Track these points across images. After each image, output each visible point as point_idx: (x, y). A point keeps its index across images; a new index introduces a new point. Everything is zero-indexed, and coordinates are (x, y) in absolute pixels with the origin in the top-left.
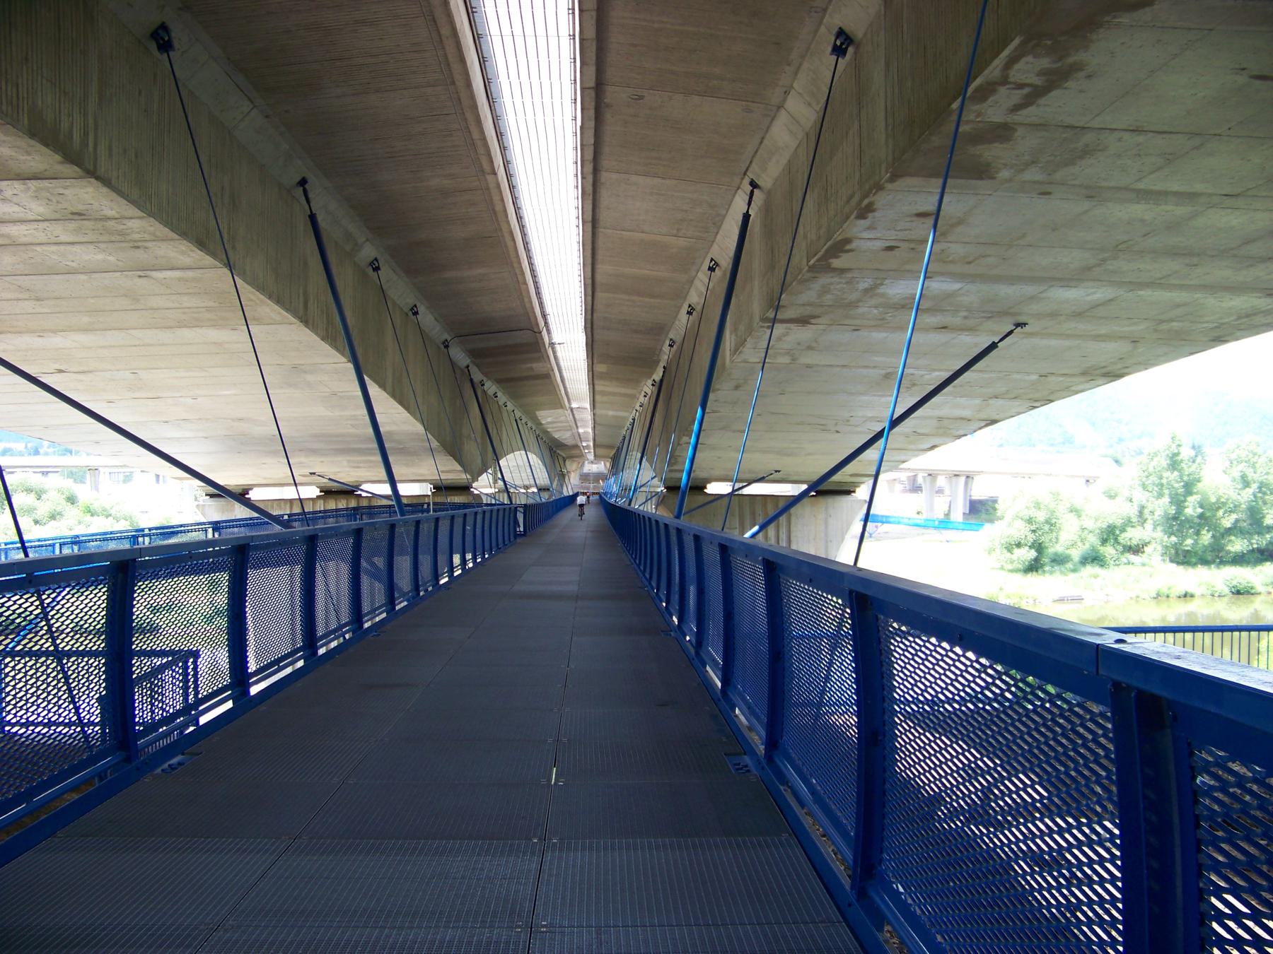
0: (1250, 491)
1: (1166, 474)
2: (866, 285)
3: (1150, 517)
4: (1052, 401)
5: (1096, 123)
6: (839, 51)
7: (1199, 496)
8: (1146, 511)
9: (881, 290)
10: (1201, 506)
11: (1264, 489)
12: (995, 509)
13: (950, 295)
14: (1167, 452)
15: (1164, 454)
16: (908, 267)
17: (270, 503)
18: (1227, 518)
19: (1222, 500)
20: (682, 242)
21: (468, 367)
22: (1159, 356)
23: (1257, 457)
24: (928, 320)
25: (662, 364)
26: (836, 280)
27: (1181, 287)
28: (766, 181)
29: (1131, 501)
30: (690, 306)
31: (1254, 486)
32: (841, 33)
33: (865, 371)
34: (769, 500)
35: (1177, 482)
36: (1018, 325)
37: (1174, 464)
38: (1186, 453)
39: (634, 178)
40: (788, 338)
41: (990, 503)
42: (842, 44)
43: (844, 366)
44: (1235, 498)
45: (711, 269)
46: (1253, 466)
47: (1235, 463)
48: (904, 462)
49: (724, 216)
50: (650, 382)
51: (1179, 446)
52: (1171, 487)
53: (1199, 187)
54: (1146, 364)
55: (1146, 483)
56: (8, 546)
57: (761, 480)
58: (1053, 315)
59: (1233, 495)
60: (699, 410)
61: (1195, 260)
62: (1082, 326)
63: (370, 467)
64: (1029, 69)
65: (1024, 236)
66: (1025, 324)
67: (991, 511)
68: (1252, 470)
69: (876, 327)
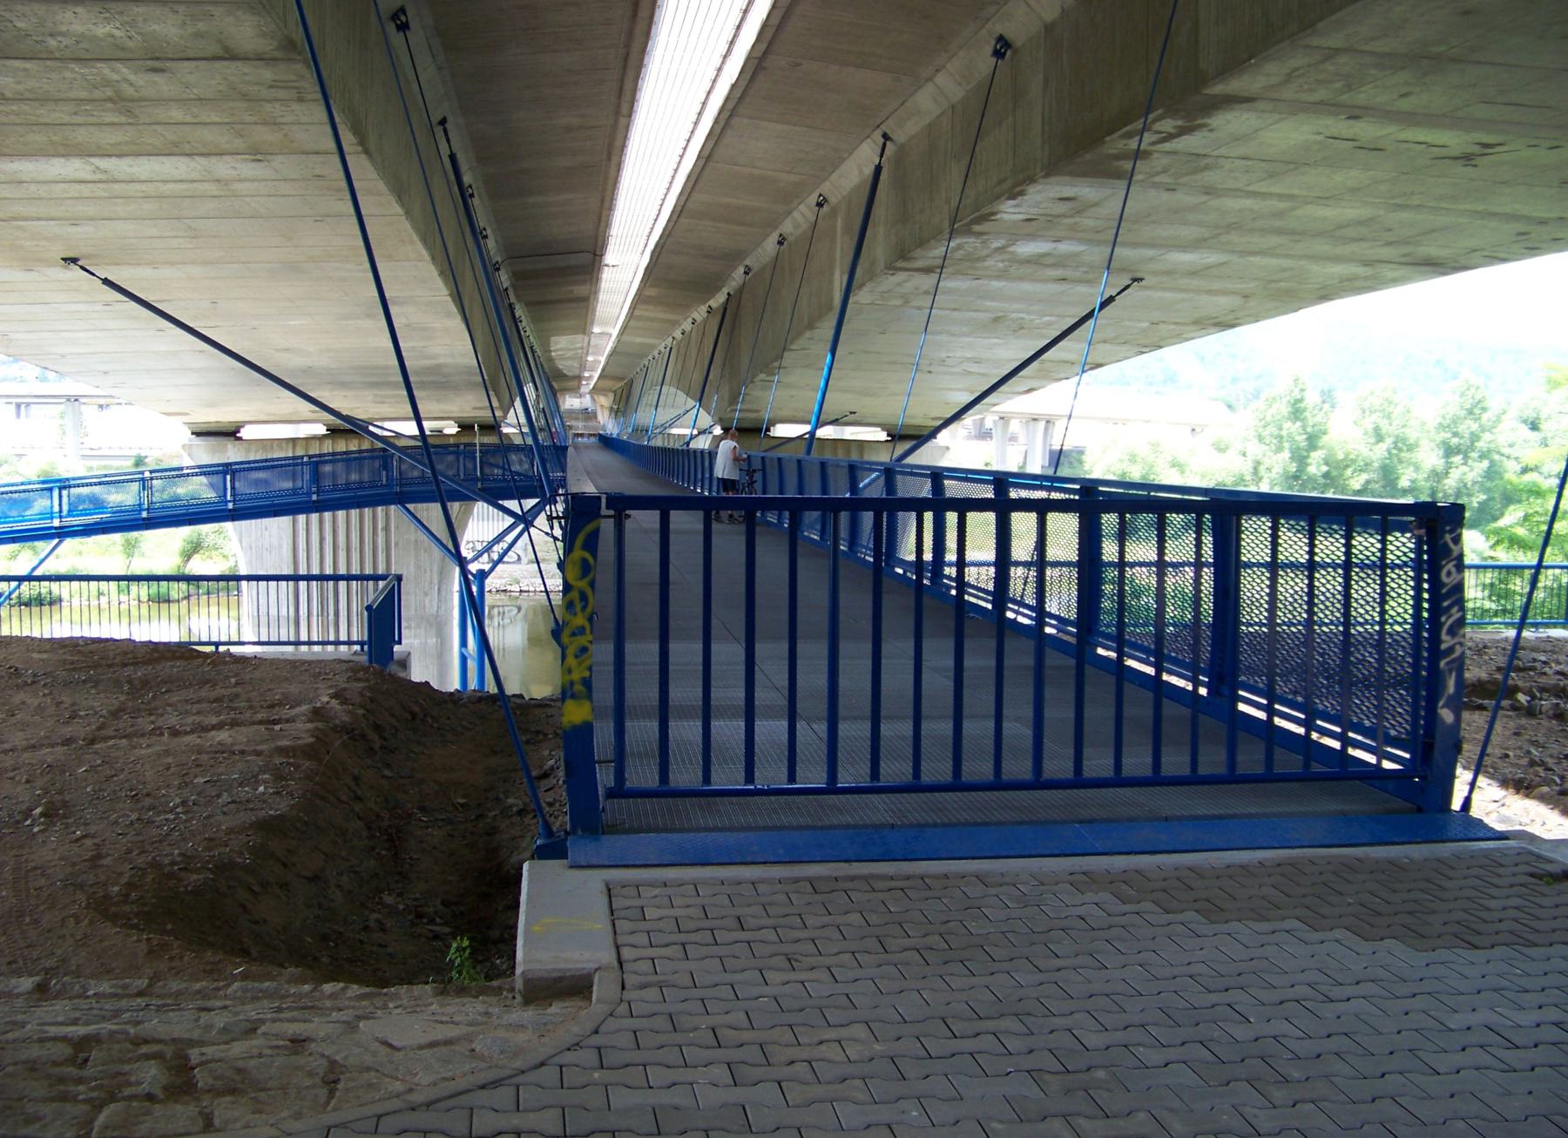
1: (1287, 425)
2: (999, 245)
3: (1266, 476)
4: (1161, 347)
5: (1216, 153)
6: (998, 54)
7: (1324, 451)
8: (1262, 469)
9: (1011, 249)
10: (1327, 464)
11: (1400, 445)
12: (1081, 462)
13: (1077, 255)
14: (1289, 398)
15: (1285, 400)
16: (1040, 233)
17: (269, 443)
18: (1356, 479)
19: (1352, 456)
20: (793, 178)
21: (507, 289)
22: (1269, 310)
23: (1392, 406)
24: (1049, 273)
25: (725, 290)
26: (972, 240)
27: (1287, 256)
28: (900, 136)
29: (1244, 455)
30: (781, 235)
31: (1389, 441)
32: (1001, 39)
33: (974, 315)
34: (839, 444)
35: (1301, 434)
36: (1135, 280)
37: (1297, 413)
38: (1312, 399)
39: (765, 124)
40: (908, 285)
41: (1074, 454)
42: (1001, 47)
43: (955, 309)
44: (1366, 455)
45: (820, 205)
46: (1389, 417)
47: (1367, 412)
48: (995, 405)
49: (845, 160)
50: (703, 309)
51: (1302, 390)
52: (1291, 438)
53: (1296, 192)
54: (1257, 318)
55: (1263, 434)
58: (1169, 273)
59: (1365, 452)
60: (829, 357)
61: (1297, 238)
62: (1195, 283)
63: (398, 403)
64: (1168, 125)
65: (1149, 215)
66: (1142, 279)
67: (1076, 464)
68: (1386, 421)
69: (998, 277)
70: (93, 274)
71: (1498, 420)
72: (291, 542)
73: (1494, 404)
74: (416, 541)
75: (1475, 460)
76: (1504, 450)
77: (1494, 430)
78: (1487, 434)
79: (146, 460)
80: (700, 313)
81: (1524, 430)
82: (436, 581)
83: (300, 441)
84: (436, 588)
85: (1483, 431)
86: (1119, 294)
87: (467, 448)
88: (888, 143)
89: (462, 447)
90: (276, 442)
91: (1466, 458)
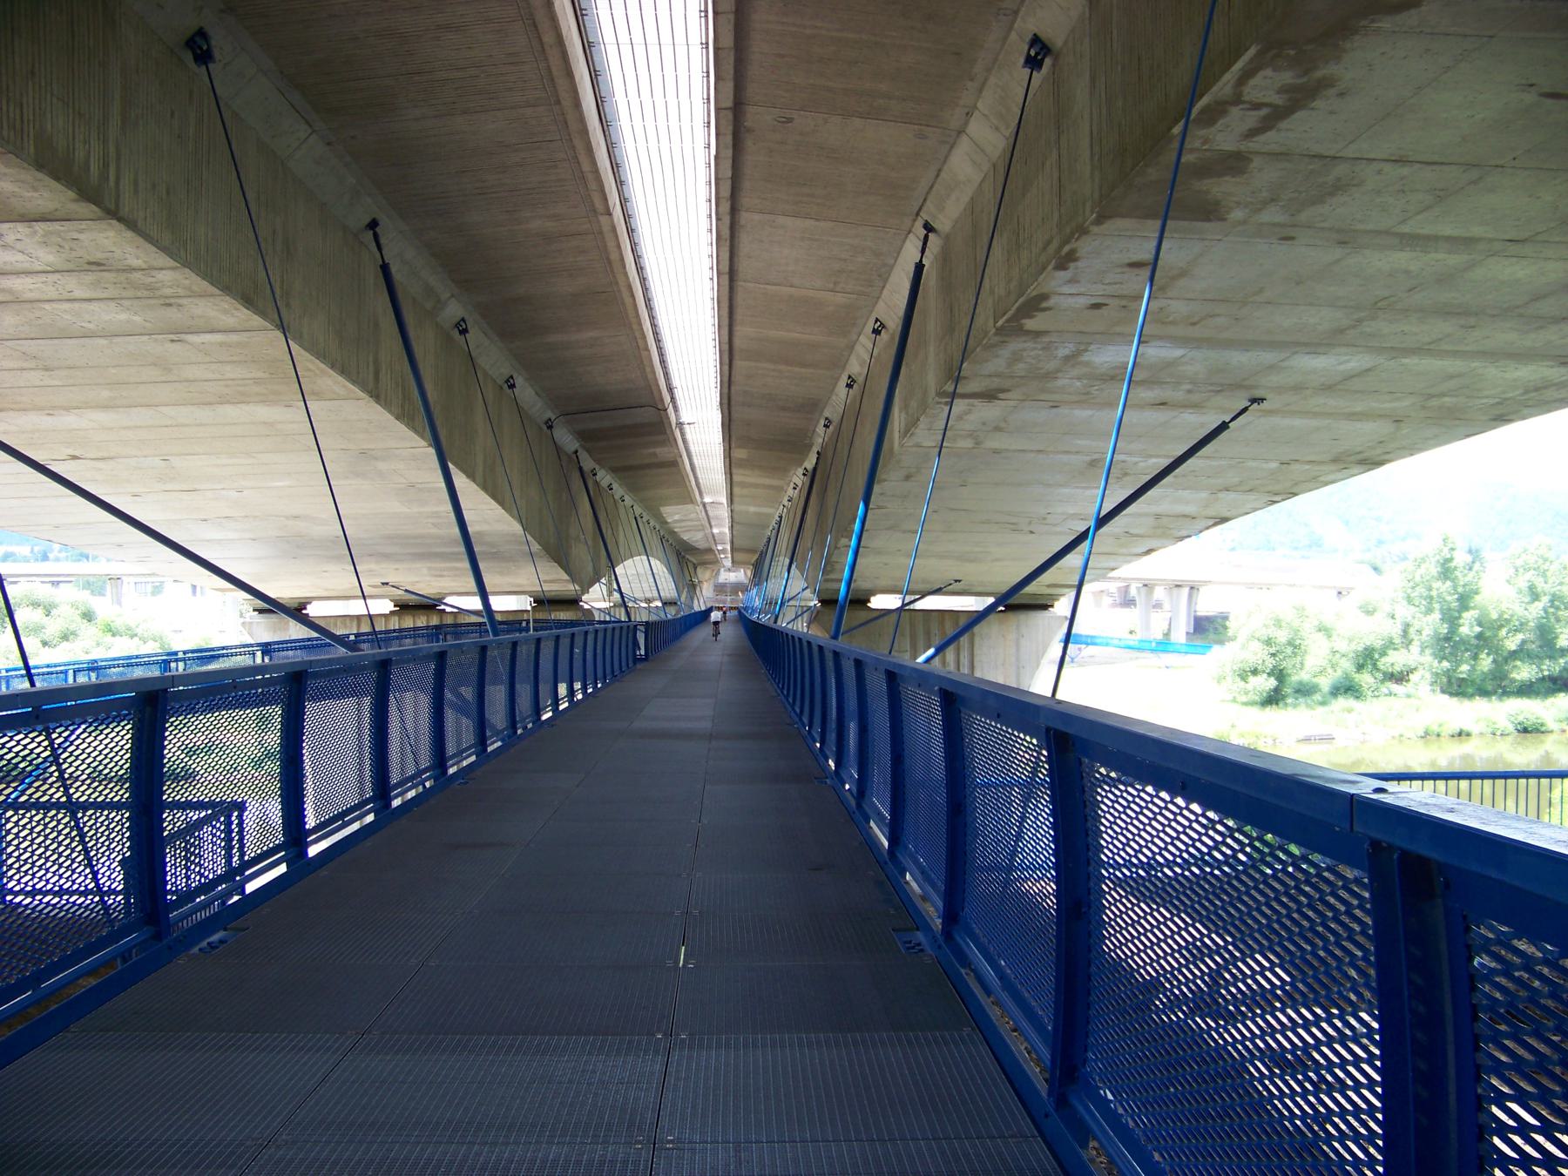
0: (1539, 605)
1: (1436, 584)
2: (1067, 352)
3: (1416, 638)
4: (1295, 494)
6: (1033, 63)
7: (1477, 611)
8: (1412, 630)
9: (1085, 358)
10: (1480, 624)
11: (1556, 603)
12: (1225, 628)
13: (1170, 364)
14: (1438, 557)
15: (1434, 560)
16: (1118, 329)
17: (332, 620)
18: (1511, 639)
19: (1506, 616)
20: (840, 299)
21: (576, 452)
22: (1427, 439)
23: (1548, 563)
24: (1143, 395)
25: (815, 449)
27: (1455, 354)
28: (943, 224)
29: (1393, 617)
30: (850, 377)
31: (1545, 600)
32: (1036, 40)
33: (1065, 458)
34: (947, 616)
35: (1450, 594)
36: (1254, 401)
37: (1446, 572)
38: (1461, 559)
39: (781, 220)
40: (971, 417)
41: (1219, 620)
42: (1037, 54)
43: (1040, 451)
44: (1521, 614)
45: (876, 332)
46: (1544, 574)
47: (1521, 570)
48: (1113, 569)
49: (892, 267)
50: (800, 471)
51: (1453, 549)
52: (1442, 600)
53: (1477, 231)
54: (1412, 449)
55: (1412, 595)
56: (10, 673)
57: (938, 591)
58: (1298, 388)
59: (1519, 610)
60: (861, 506)
61: (1472, 321)
62: (1333, 402)
63: (456, 576)
64: (1267, 85)
65: (1261, 290)
66: (1263, 400)
67: (1221, 629)
69: (1079, 403)
80: (798, 478)
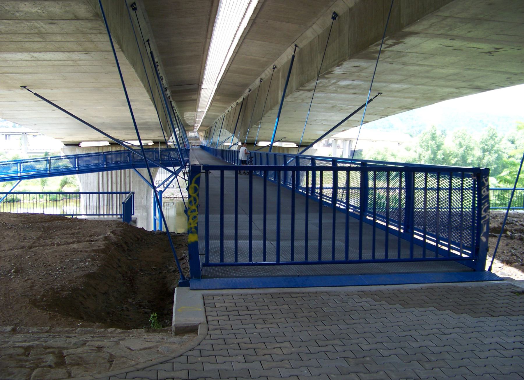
1: (430, 142)
2: (334, 82)
3: (423, 159)
4: (388, 116)
6: (334, 18)
7: (443, 151)
8: (422, 157)
9: (338, 83)
10: (443, 155)
11: (468, 149)
12: (361, 154)
13: (360, 85)
14: (431, 133)
15: (429, 134)
16: (347, 78)
17: (90, 148)
18: (453, 160)
19: (452, 152)
20: (265, 59)
21: (169, 96)
22: (424, 103)
23: (465, 136)
24: (351, 91)
25: (242, 97)
27: (430, 86)
28: (301, 46)
29: (416, 152)
30: (261, 79)
31: (464, 147)
32: (334, 13)
33: (326, 105)
34: (280, 148)
35: (435, 145)
36: (379, 93)
37: (433, 138)
38: (438, 133)
39: (256, 41)
40: (303, 95)
41: (359, 152)
42: (335, 16)
43: (319, 103)
44: (456, 152)
45: (274, 68)
46: (464, 139)
47: (457, 138)
48: (332, 135)
49: (282, 53)
50: (235, 103)
51: (435, 130)
52: (431, 146)
53: (433, 64)
54: (420, 106)
55: (422, 145)
58: (391, 91)
59: (456, 151)
60: (277, 119)
61: (434, 79)
62: (399, 94)
63: (133, 134)
64: (390, 42)
65: (384, 72)
66: (382, 93)
67: (360, 155)
68: (463, 141)
69: (334, 93)
70: (31, 92)
71: (501, 140)
72: (97, 181)
73: (499, 135)
74: (139, 181)
75: (493, 154)
76: (502, 150)
77: (499, 144)
78: (497, 145)
79: (49, 154)
80: (234, 105)
81: (509, 144)
82: (146, 194)
83: (100, 147)
84: (146, 196)
85: (496, 144)
86: (374, 98)
87: (156, 150)
88: (297, 48)
89: (154, 149)
90: (92, 148)
91: (490, 153)
